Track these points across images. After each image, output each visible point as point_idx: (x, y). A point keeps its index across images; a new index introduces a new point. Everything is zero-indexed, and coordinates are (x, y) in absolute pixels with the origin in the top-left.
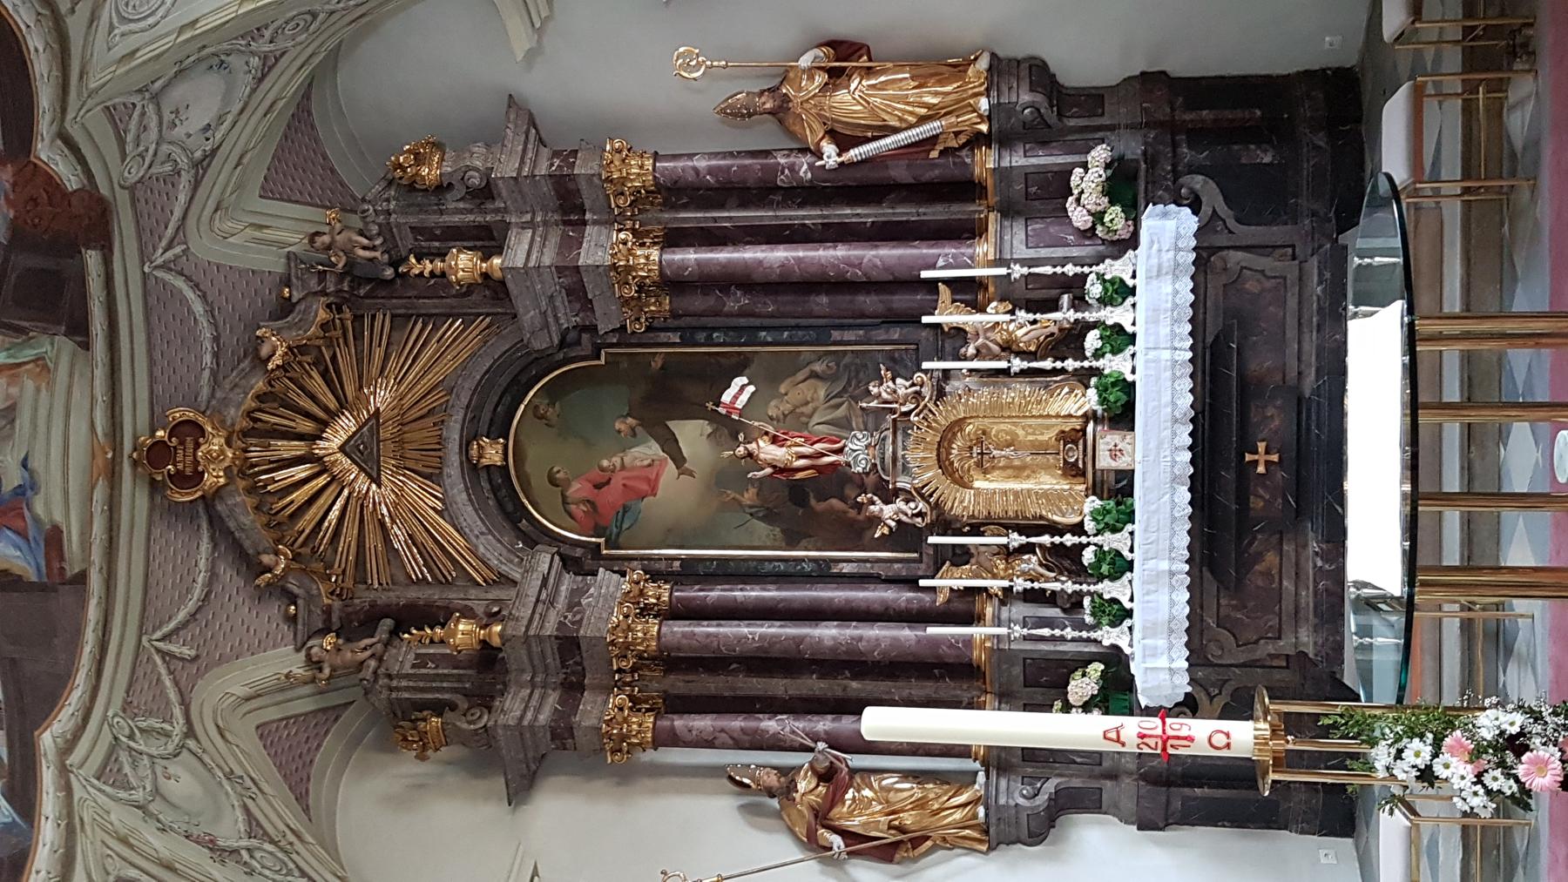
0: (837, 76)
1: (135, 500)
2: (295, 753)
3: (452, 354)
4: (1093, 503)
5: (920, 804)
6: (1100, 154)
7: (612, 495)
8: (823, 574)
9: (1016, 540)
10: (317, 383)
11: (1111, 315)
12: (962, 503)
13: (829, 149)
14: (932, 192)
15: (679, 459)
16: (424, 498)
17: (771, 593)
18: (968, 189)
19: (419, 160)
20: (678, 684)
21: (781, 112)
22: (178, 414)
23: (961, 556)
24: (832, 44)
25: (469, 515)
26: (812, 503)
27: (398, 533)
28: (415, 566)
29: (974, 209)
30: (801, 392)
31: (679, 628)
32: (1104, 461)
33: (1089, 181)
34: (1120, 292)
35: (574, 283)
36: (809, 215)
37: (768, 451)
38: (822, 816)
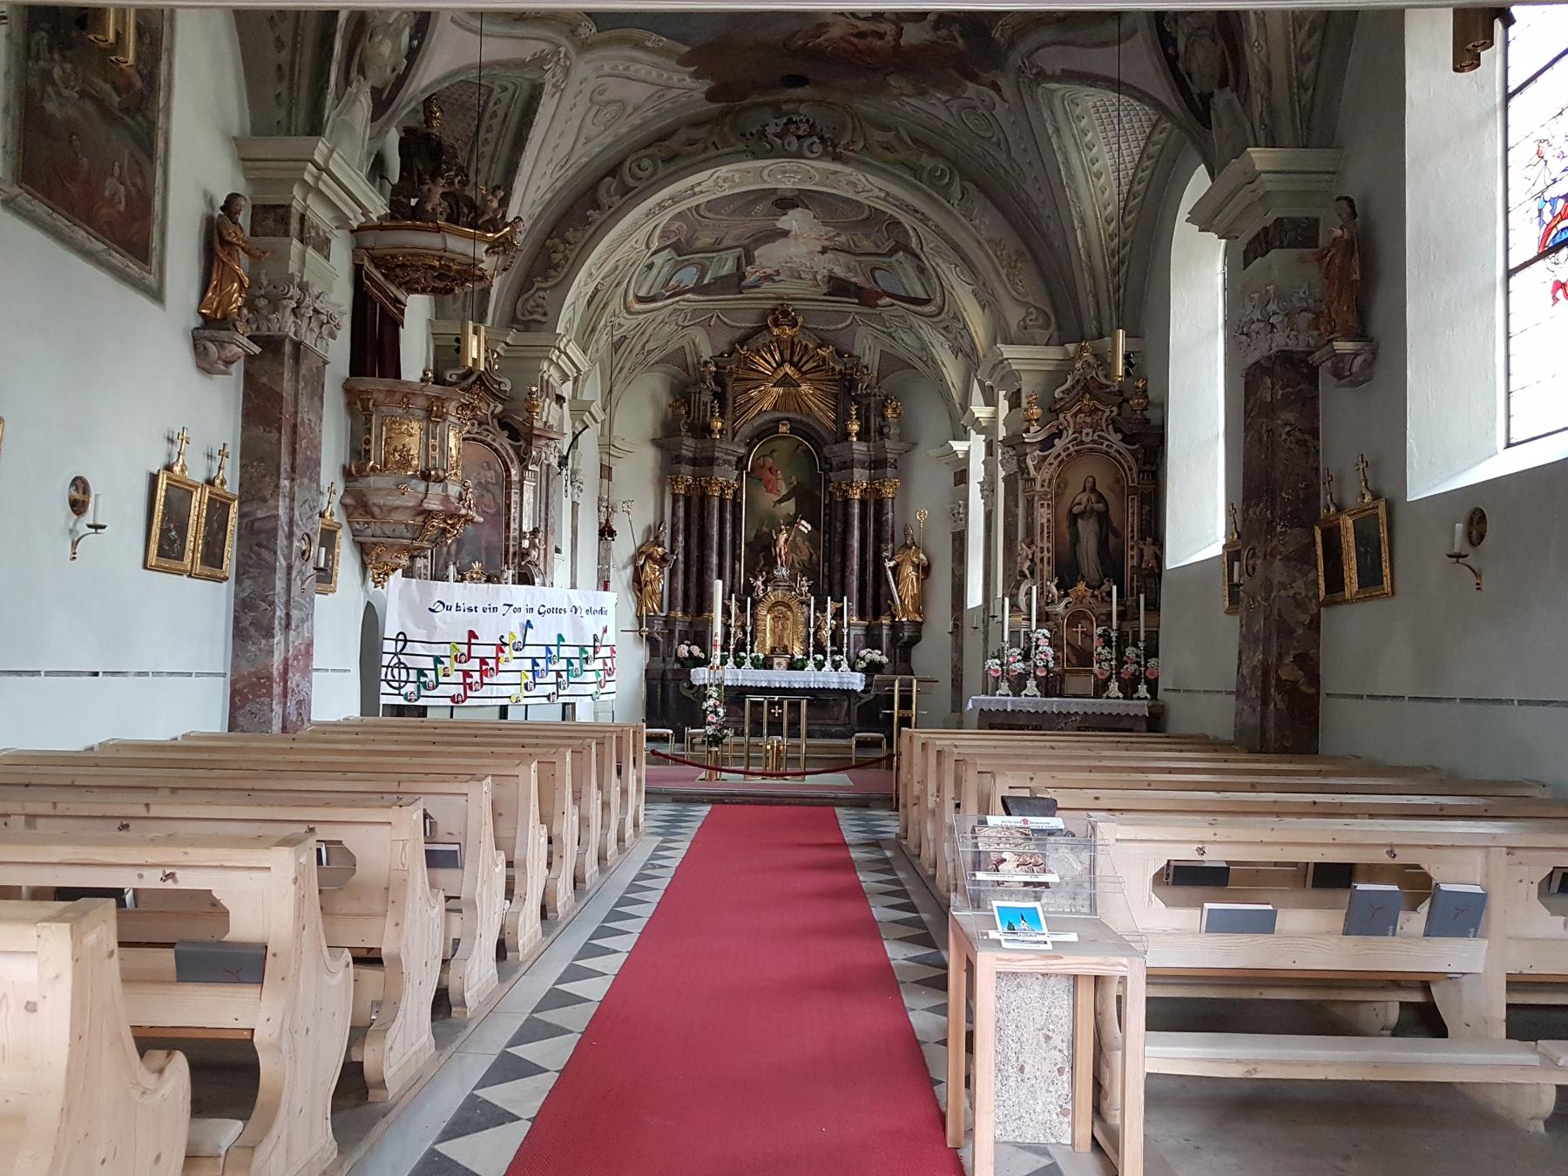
0: (916, 567)
1: (769, 305)
2: (676, 358)
3: (822, 413)
4: (762, 656)
5: (654, 592)
6: (885, 659)
7: (768, 475)
8: (735, 558)
9: (749, 629)
10: (811, 365)
11: (828, 664)
12: (762, 611)
13: (892, 564)
14: (875, 602)
15: (780, 502)
16: (766, 405)
17: (728, 538)
18: (877, 616)
19: (894, 410)
20: (695, 501)
21: (906, 547)
22: (800, 320)
23: (742, 609)
24: (929, 566)
25: (760, 421)
26: (762, 554)
27: (754, 393)
28: (741, 400)
29: (870, 617)
30: (805, 550)
31: (716, 503)
32: (776, 660)
33: (876, 655)
34: (836, 666)
35: (848, 465)
36: (870, 555)
37: (783, 537)
38: (649, 557)
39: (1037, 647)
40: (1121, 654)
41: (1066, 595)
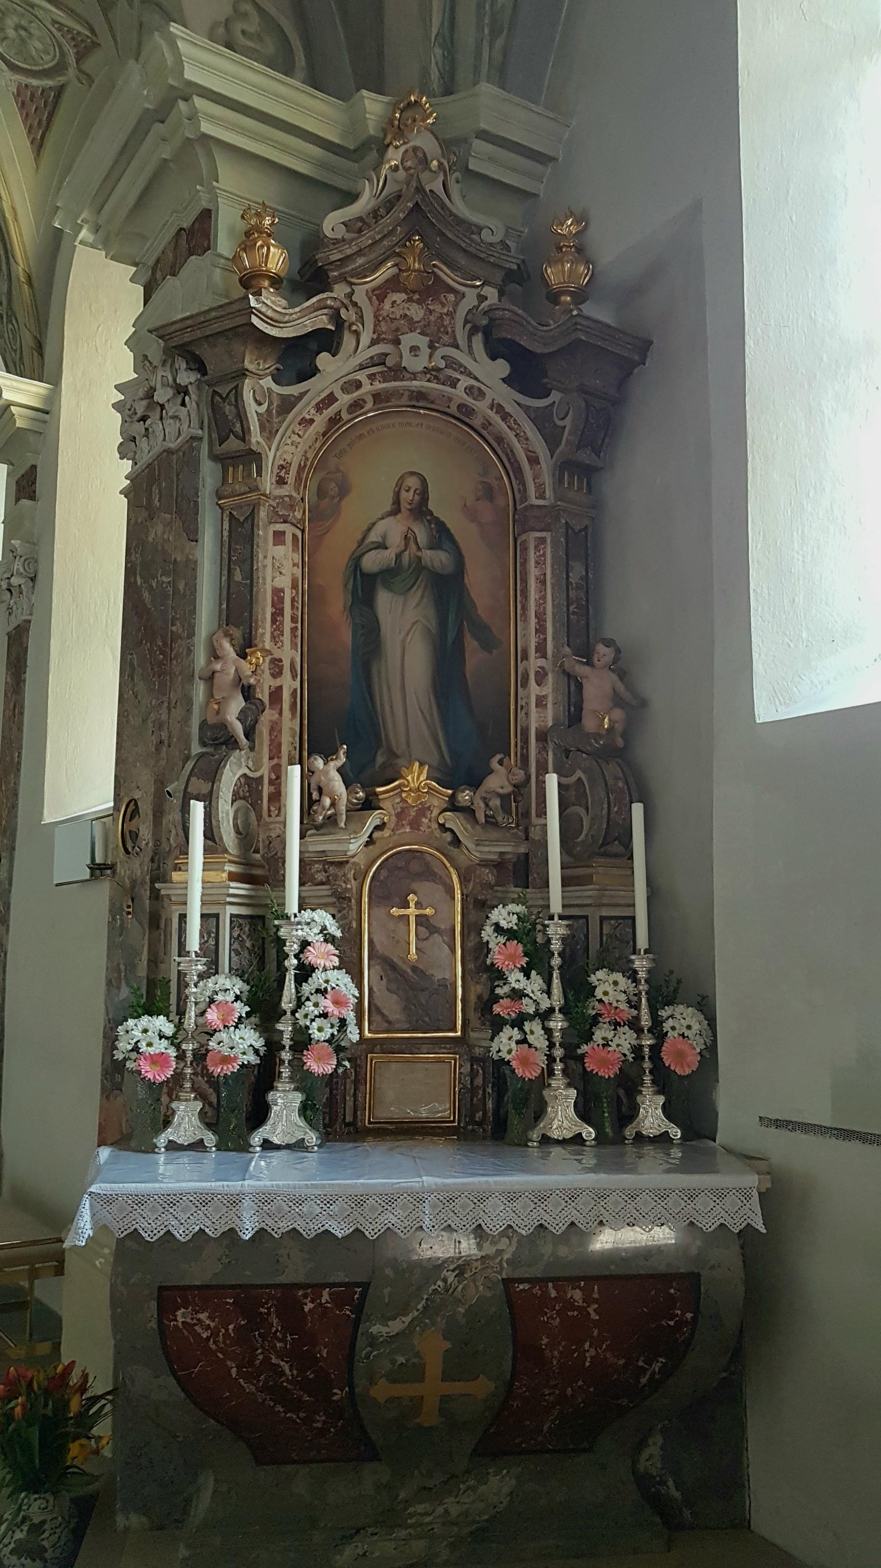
39: (305, 972)
40: (578, 988)
41: (369, 804)
